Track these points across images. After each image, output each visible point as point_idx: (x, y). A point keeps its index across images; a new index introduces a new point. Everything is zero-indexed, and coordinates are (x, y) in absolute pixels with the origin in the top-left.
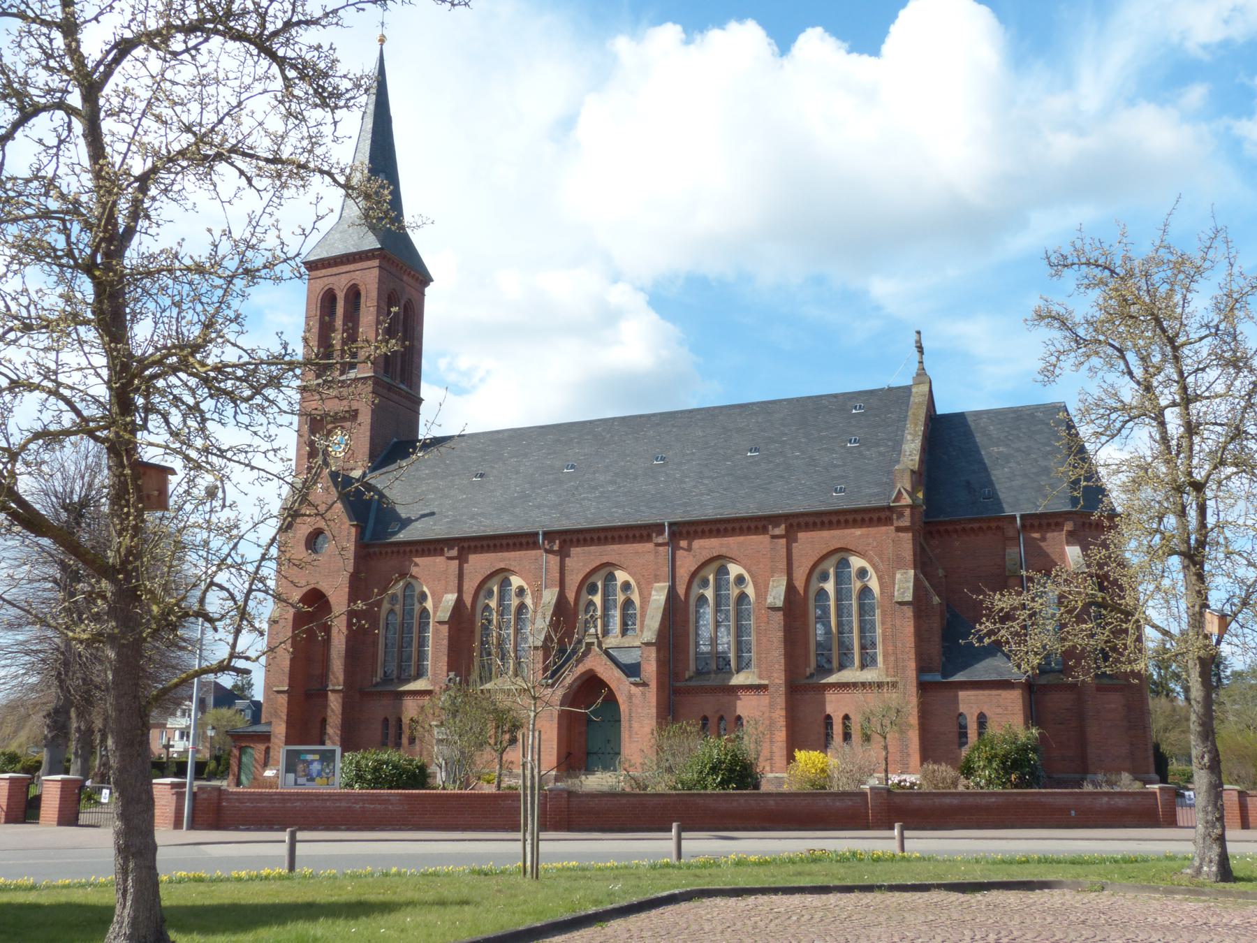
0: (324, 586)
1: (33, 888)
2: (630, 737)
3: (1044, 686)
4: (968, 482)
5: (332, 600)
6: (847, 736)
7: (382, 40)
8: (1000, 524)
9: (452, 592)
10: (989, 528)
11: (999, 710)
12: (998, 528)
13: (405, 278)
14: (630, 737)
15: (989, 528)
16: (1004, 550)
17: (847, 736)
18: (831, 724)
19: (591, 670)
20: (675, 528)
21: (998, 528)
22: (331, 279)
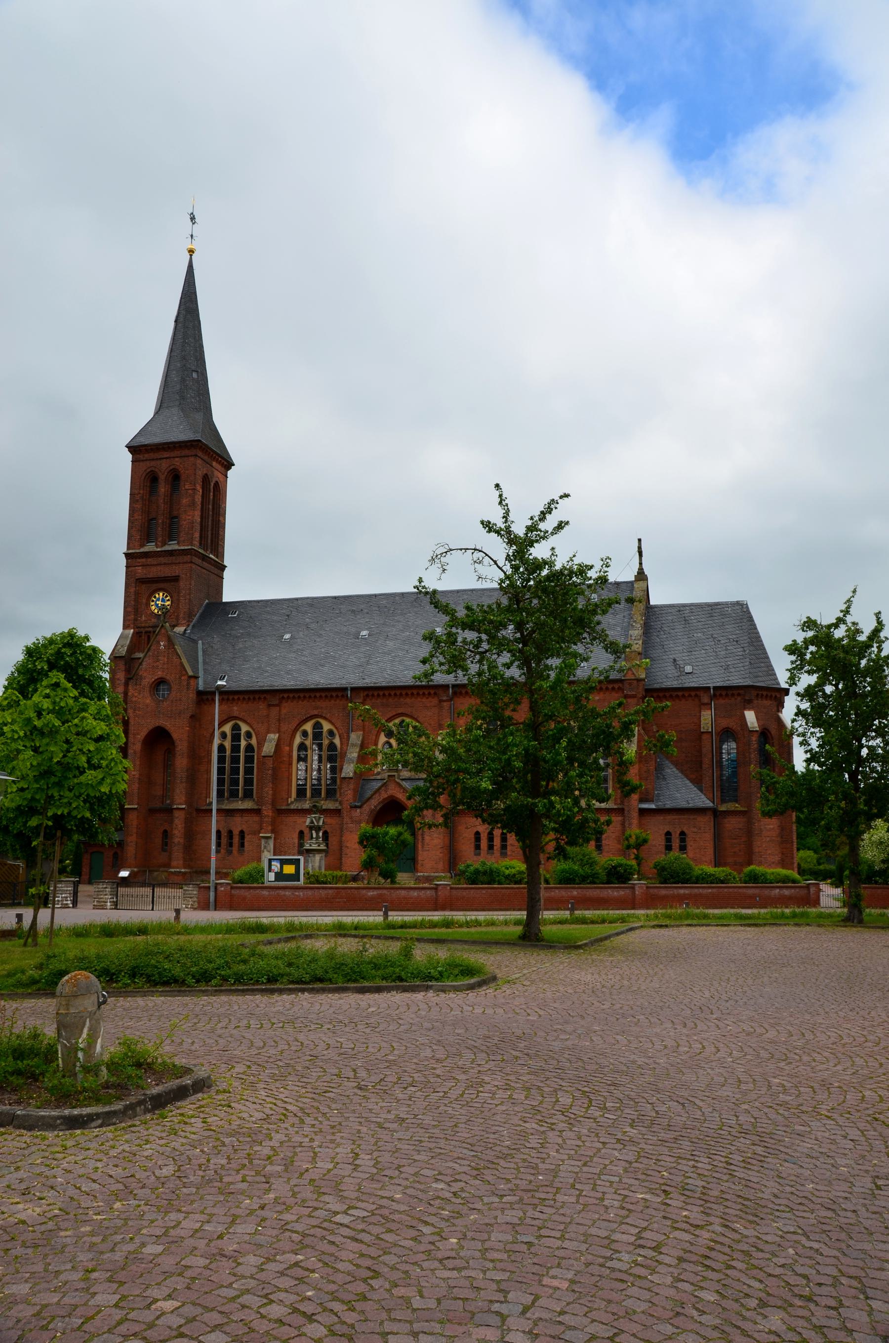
0: (167, 724)
1: (736, 932)
2: (423, 847)
3: (724, 811)
4: (675, 660)
5: (175, 736)
6: (491, 847)
7: (191, 252)
8: (698, 693)
9: (274, 733)
10: (690, 696)
11: (695, 830)
12: (696, 695)
13: (214, 464)
14: (423, 847)
15: (613, 689)
16: (700, 712)
17: (491, 847)
18: (493, 838)
19: (392, 796)
20: (456, 689)
21: (619, 688)
22: (153, 463)
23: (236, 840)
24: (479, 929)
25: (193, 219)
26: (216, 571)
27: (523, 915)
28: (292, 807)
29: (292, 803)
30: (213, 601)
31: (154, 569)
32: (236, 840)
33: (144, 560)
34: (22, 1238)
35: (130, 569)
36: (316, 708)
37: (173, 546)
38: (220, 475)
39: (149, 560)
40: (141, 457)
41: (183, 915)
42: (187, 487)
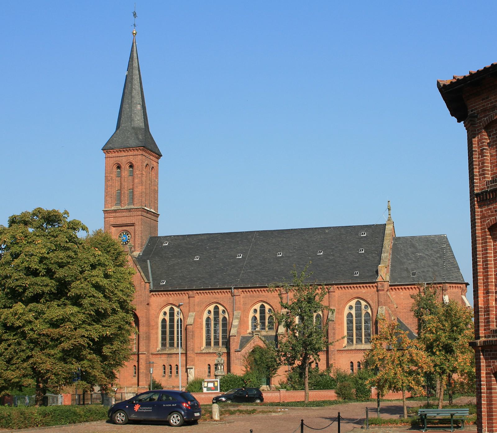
22: (117, 159)
23: (174, 370)
24: (151, 286)
25: (135, 15)
26: (154, 218)
27: (474, 400)
28: (204, 352)
29: (204, 349)
30: (153, 235)
31: (120, 219)
32: (174, 370)
33: (114, 214)
34: (382, 342)
35: (107, 219)
36: (215, 298)
37: (132, 207)
38: (154, 163)
39: (117, 214)
40: (110, 155)
41: (405, 403)
42: (137, 173)
